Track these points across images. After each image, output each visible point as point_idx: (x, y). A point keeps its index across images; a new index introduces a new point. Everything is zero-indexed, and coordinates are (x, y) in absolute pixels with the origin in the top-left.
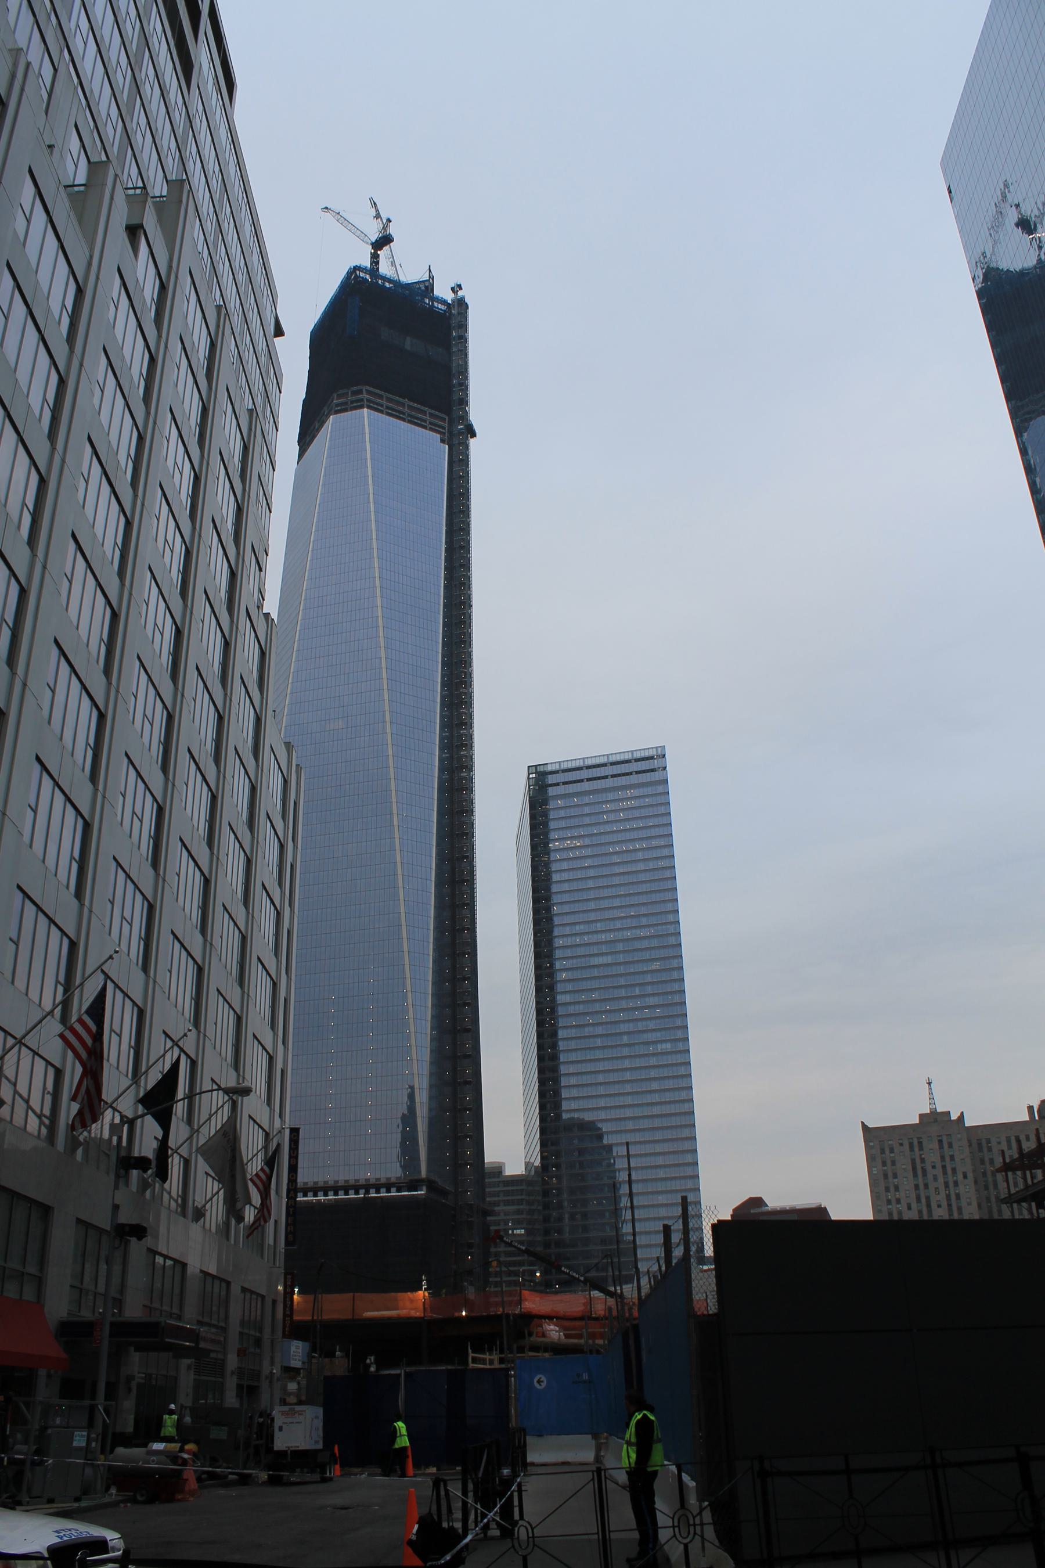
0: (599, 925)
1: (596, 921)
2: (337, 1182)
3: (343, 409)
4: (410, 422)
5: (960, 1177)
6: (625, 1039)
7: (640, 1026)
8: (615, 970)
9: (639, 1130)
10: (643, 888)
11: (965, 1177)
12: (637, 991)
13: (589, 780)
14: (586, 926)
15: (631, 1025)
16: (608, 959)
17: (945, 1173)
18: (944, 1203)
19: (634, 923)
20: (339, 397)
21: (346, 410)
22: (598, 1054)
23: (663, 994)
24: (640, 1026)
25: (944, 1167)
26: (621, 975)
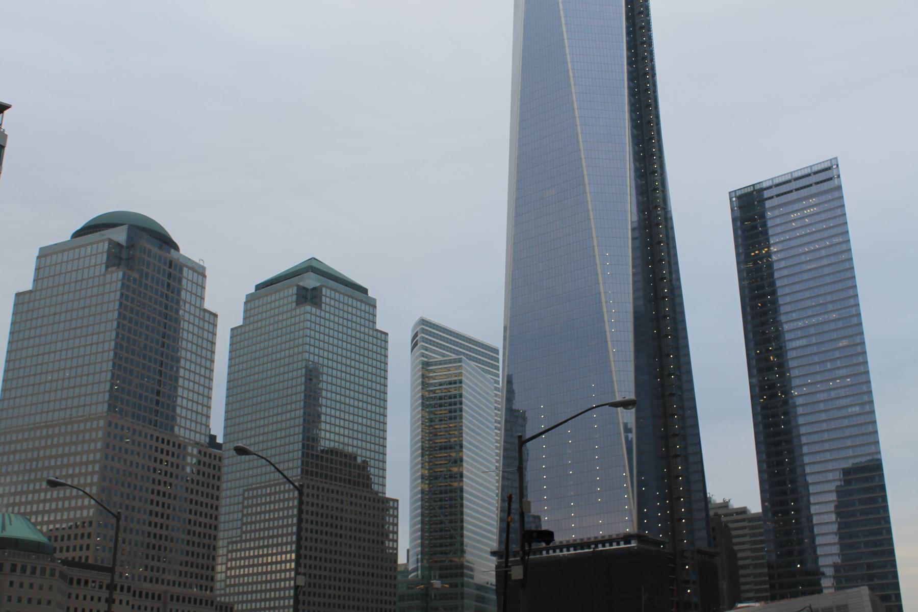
6: (822, 406)
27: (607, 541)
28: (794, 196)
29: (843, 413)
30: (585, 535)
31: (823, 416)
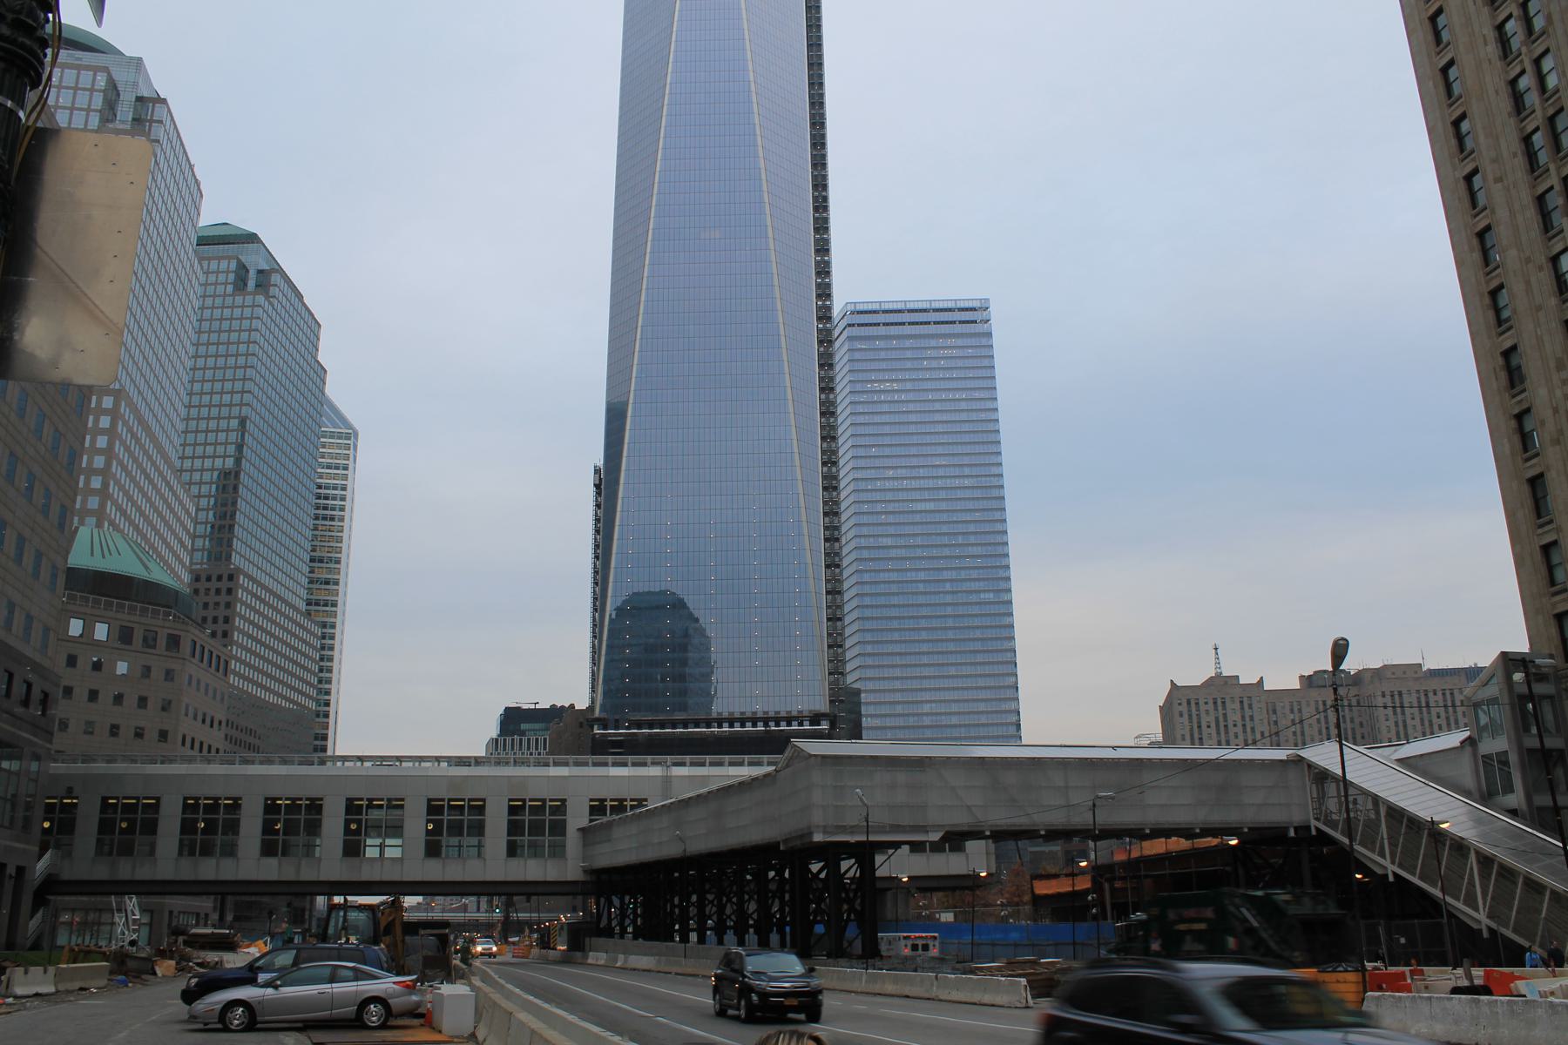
6: (948, 587)
16: (931, 506)
19: (957, 472)
22: (921, 600)
27: (749, 719)
28: (932, 329)
29: (973, 598)
30: (759, 708)
31: (949, 599)
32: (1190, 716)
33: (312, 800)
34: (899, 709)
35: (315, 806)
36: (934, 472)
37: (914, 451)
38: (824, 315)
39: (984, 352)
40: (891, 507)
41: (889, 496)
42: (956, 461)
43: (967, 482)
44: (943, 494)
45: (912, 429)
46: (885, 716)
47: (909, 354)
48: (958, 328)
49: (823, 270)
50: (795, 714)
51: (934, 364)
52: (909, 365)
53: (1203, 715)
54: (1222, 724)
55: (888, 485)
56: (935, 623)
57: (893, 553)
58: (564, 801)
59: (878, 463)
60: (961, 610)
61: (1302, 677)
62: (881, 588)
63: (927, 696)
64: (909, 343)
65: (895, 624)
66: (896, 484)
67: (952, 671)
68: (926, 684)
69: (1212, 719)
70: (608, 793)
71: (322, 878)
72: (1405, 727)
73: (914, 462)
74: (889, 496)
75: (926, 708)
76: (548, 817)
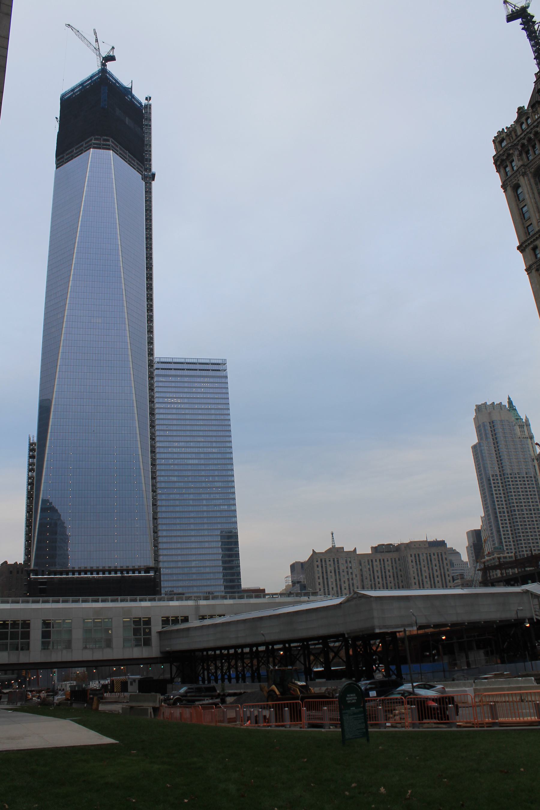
0: (192, 444)
1: (191, 442)
2: (105, 567)
3: (98, 147)
4: (129, 164)
5: (354, 576)
6: (204, 502)
7: (212, 496)
8: (200, 468)
9: (211, 548)
10: (214, 428)
11: (356, 576)
12: (211, 479)
13: (213, 370)
14: (185, 443)
15: (208, 495)
16: (196, 462)
17: (348, 574)
18: (347, 588)
19: (209, 445)
20: (96, 139)
21: (100, 148)
22: (191, 509)
23: (223, 481)
24: (212, 496)
25: (347, 572)
26: (203, 470)
27: (113, 570)
30: (117, 564)
31: (205, 508)
32: (322, 567)
33: (24, 621)
34: (180, 564)
35: (26, 624)
36: (198, 445)
37: (188, 433)
38: (151, 364)
39: (223, 385)
40: (176, 462)
41: (175, 456)
42: (209, 439)
43: (214, 450)
44: (202, 456)
45: (188, 422)
46: (173, 568)
47: (186, 385)
48: (211, 373)
49: (151, 342)
50: (136, 567)
51: (199, 390)
52: (186, 390)
53: (328, 566)
54: (337, 571)
55: (175, 450)
56: (198, 521)
57: (177, 485)
58: (150, 618)
59: (170, 439)
60: (211, 515)
61: (372, 548)
62: (172, 503)
63: (194, 558)
64: (186, 379)
65: (178, 521)
66: (178, 450)
67: (207, 545)
68: (193, 552)
69: (332, 568)
70: (171, 614)
71: (31, 662)
72: (421, 571)
73: (188, 439)
74: (175, 456)
75: (193, 564)
76: (142, 626)
